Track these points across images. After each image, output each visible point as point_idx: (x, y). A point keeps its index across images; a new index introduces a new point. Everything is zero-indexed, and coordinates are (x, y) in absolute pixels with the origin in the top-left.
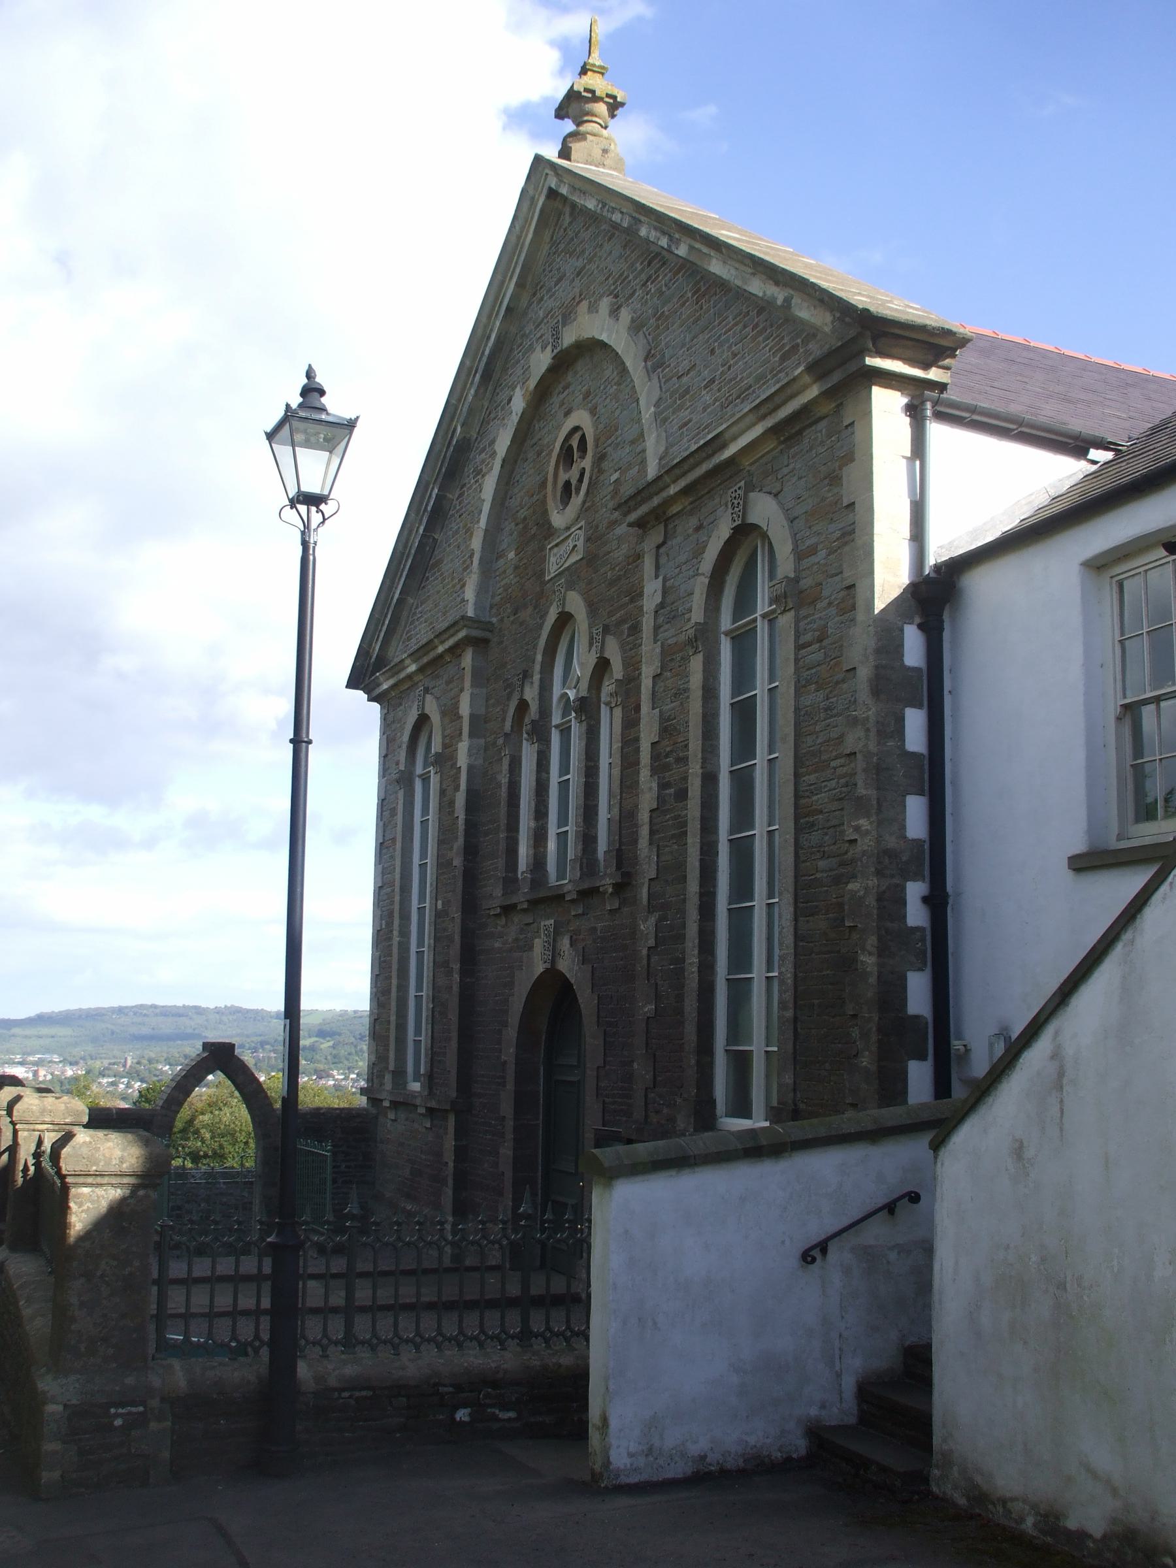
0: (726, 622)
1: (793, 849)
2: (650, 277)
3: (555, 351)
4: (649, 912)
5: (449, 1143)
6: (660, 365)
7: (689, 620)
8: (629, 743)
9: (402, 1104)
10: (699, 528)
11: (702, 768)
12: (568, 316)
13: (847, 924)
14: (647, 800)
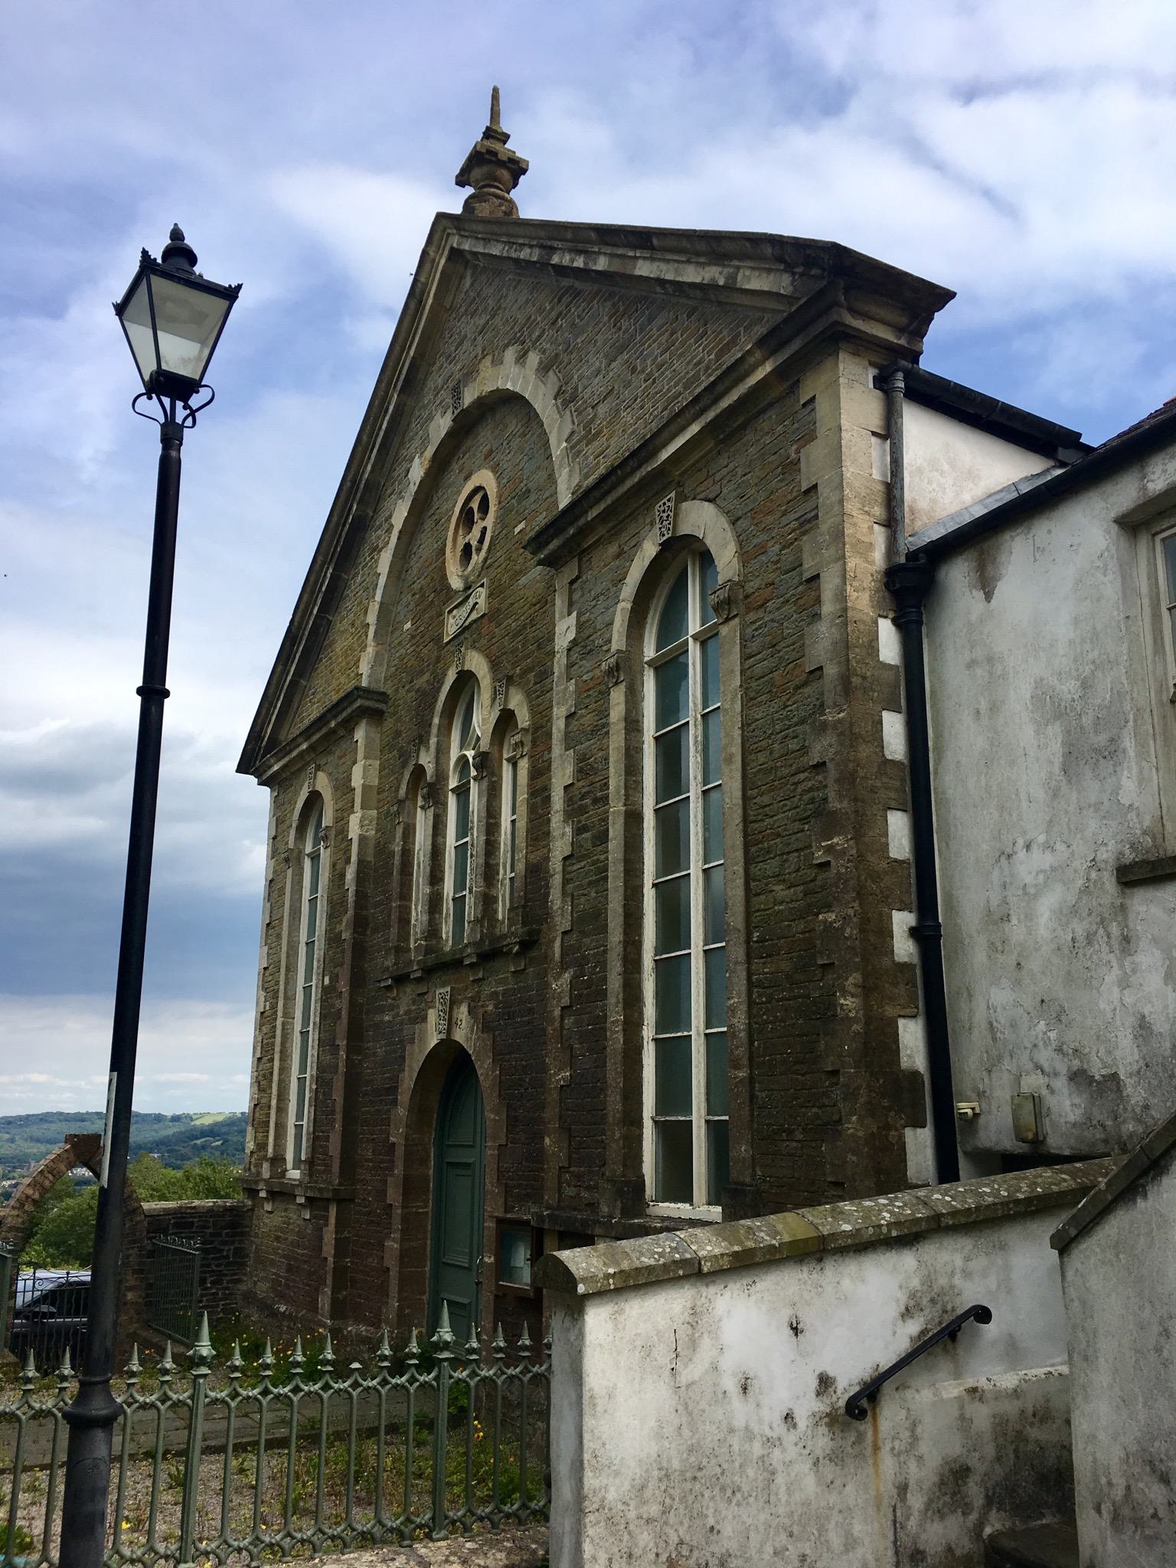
0: (650, 652)
1: (742, 880)
2: (560, 314)
3: (456, 412)
4: (562, 968)
5: (329, 1235)
6: (573, 398)
7: (609, 650)
8: (539, 795)
9: (281, 1194)
10: (618, 556)
11: (625, 805)
12: (470, 373)
13: (820, 962)
14: (561, 842)
